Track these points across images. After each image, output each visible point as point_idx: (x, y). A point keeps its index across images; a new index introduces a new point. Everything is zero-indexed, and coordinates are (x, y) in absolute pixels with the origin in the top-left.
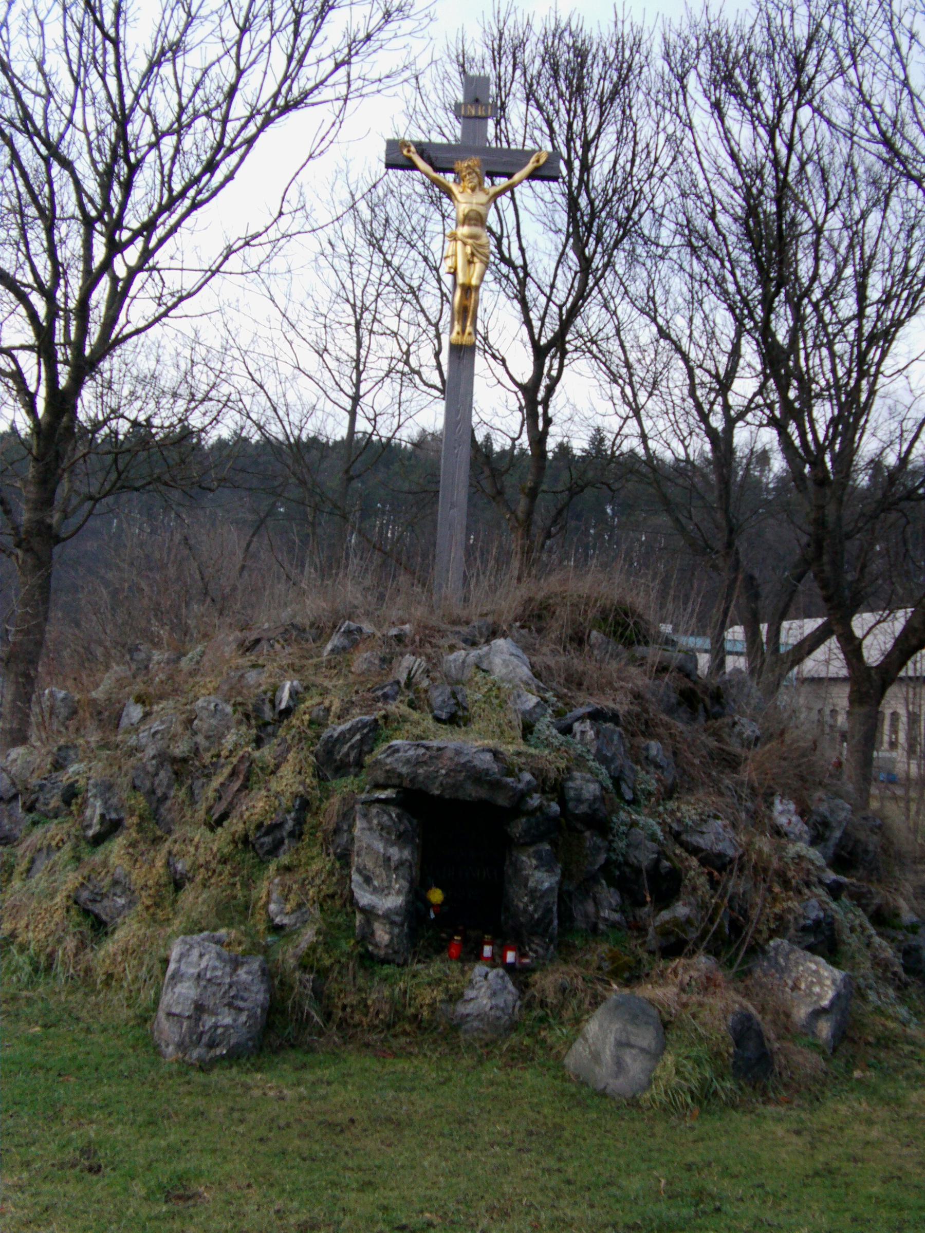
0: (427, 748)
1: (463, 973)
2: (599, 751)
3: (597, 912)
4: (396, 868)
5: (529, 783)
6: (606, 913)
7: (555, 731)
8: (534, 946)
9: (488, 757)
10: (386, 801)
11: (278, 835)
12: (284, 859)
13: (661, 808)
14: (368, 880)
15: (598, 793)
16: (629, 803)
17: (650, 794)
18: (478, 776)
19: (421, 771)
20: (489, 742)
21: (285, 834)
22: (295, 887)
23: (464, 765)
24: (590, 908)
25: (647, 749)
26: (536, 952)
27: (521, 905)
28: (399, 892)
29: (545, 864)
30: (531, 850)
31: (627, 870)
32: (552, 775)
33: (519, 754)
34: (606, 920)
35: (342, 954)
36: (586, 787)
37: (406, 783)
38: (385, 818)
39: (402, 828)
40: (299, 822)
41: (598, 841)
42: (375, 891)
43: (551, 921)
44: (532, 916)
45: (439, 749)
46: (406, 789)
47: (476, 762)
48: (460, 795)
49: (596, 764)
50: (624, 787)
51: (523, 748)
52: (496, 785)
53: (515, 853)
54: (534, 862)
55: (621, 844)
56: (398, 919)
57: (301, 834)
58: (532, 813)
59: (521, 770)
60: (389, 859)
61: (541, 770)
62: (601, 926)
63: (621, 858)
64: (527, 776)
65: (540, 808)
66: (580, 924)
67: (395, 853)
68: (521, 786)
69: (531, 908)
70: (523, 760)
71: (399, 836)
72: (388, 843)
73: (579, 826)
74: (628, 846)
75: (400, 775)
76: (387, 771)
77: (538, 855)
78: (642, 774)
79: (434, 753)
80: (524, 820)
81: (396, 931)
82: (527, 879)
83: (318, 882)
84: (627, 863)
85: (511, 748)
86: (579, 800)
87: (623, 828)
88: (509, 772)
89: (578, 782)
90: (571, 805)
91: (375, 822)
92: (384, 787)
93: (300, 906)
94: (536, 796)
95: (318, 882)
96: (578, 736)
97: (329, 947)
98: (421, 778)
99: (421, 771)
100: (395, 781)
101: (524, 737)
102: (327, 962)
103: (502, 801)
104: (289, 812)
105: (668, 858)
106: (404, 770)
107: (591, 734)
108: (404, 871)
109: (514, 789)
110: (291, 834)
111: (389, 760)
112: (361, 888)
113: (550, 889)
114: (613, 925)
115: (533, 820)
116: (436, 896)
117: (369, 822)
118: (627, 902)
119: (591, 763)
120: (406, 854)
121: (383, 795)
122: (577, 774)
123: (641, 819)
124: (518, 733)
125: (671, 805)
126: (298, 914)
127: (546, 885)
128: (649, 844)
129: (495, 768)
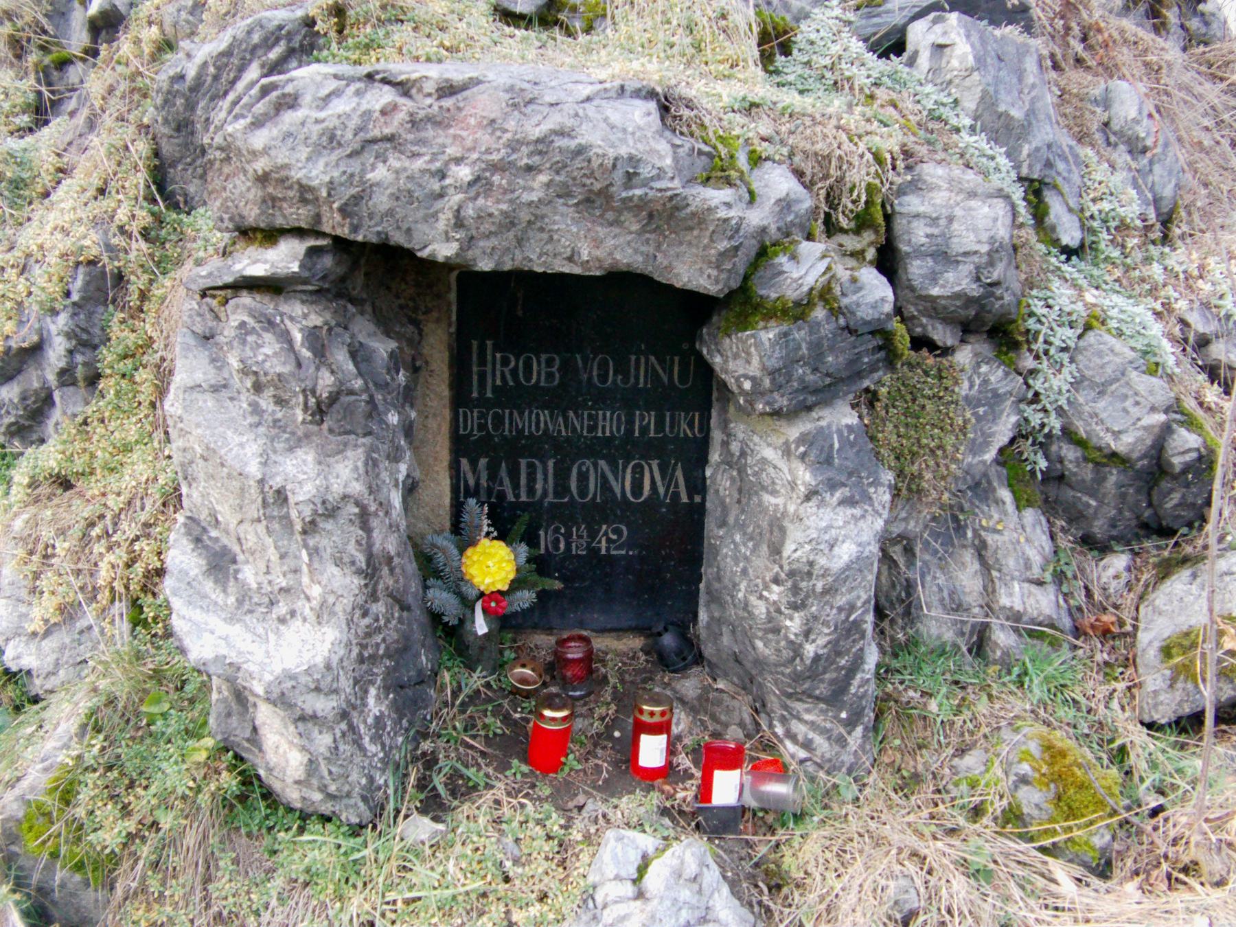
0: (404, 88)
1: (563, 854)
2: (988, 101)
3: (989, 590)
4: (310, 528)
5: (785, 204)
6: (1014, 596)
7: (857, 46)
8: (799, 728)
9: (642, 114)
10: (271, 286)
11: (32, 379)
12: (48, 456)
13: (1156, 270)
14: (221, 564)
15: (1003, 232)
16: (1069, 252)
17: (1123, 227)
18: (602, 192)
19: (380, 173)
20: (654, 71)
21: (51, 378)
22: (61, 547)
23: (542, 145)
24: (968, 578)
25: (1106, 102)
26: (807, 745)
27: (760, 609)
28: (323, 613)
29: (838, 475)
30: (794, 431)
31: (1070, 453)
32: (860, 175)
33: (751, 108)
34: (1016, 617)
35: (165, 801)
36: (963, 214)
37: (333, 223)
38: (270, 346)
39: (326, 382)
40: (86, 341)
41: (995, 375)
42: (246, 604)
43: (857, 662)
44: (797, 650)
45: (448, 90)
46: (341, 244)
47: (591, 136)
48: (539, 258)
49: (980, 142)
50: (1056, 209)
51: (761, 88)
52: (665, 217)
53: (739, 429)
54: (805, 477)
55: (1054, 382)
56: (324, 706)
57: (93, 379)
58: (798, 311)
59: (756, 160)
60: (281, 496)
61: (824, 160)
62: (1002, 637)
63: (1055, 423)
64: (777, 182)
65: (824, 294)
66: (936, 625)
67: (306, 474)
68: (756, 217)
69: (793, 624)
70: (764, 127)
71: (320, 412)
72: (283, 437)
73: (942, 334)
74: (1076, 384)
75: (305, 193)
76: (263, 179)
77: (818, 452)
78: (1100, 172)
79: (426, 104)
80: (769, 335)
81: (323, 741)
82: (778, 527)
83: (129, 529)
84: (1068, 434)
85: (730, 92)
86: (943, 256)
87: (1066, 335)
88: (717, 170)
89: (940, 197)
90: (916, 270)
91: (234, 362)
92: (271, 235)
93: (68, 612)
94: (811, 250)
95: (129, 529)
96: (924, 61)
97: (122, 781)
98: (381, 201)
99: (380, 173)
100: (299, 215)
101: (766, 59)
102: (110, 836)
103: (692, 270)
104: (54, 312)
105: (1190, 423)
106: (318, 173)
107: (963, 51)
108: (340, 536)
109: (732, 229)
110: (66, 376)
111: (259, 139)
112: (197, 598)
113: (856, 566)
114: (1034, 631)
115: (800, 334)
116: (492, 565)
117: (217, 361)
118: (1064, 542)
119: (966, 138)
120: (346, 475)
121: (259, 262)
122: (932, 172)
123: (1116, 304)
124: (750, 49)
125: (1181, 258)
126: (63, 637)
127: (846, 552)
128: (1142, 382)
129: (660, 153)
